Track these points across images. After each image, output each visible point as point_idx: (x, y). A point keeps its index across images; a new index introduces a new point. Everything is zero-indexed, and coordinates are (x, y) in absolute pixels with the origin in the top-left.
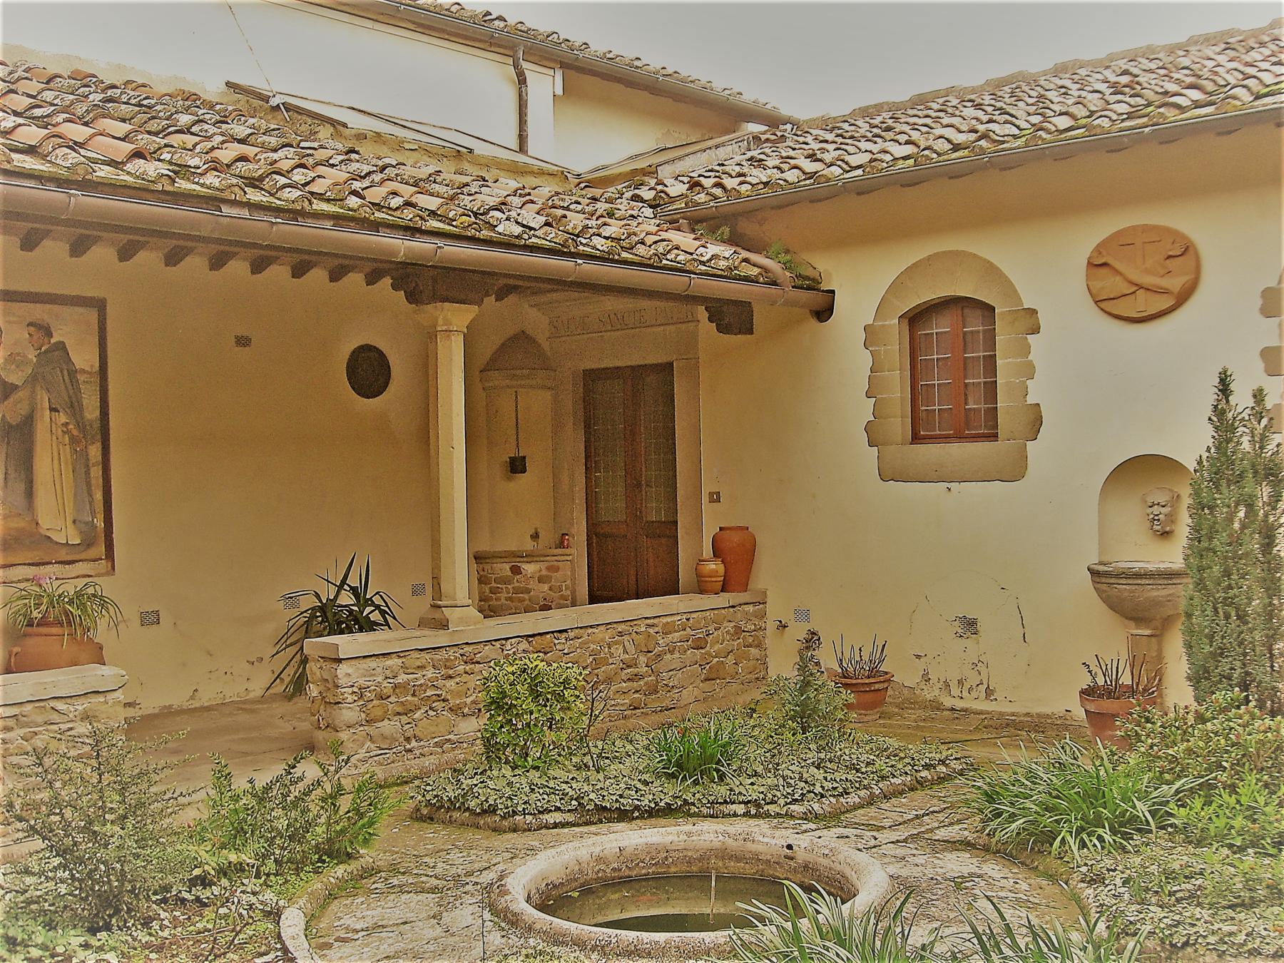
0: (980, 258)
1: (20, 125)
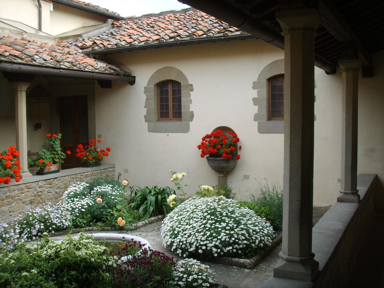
0: (177, 69)
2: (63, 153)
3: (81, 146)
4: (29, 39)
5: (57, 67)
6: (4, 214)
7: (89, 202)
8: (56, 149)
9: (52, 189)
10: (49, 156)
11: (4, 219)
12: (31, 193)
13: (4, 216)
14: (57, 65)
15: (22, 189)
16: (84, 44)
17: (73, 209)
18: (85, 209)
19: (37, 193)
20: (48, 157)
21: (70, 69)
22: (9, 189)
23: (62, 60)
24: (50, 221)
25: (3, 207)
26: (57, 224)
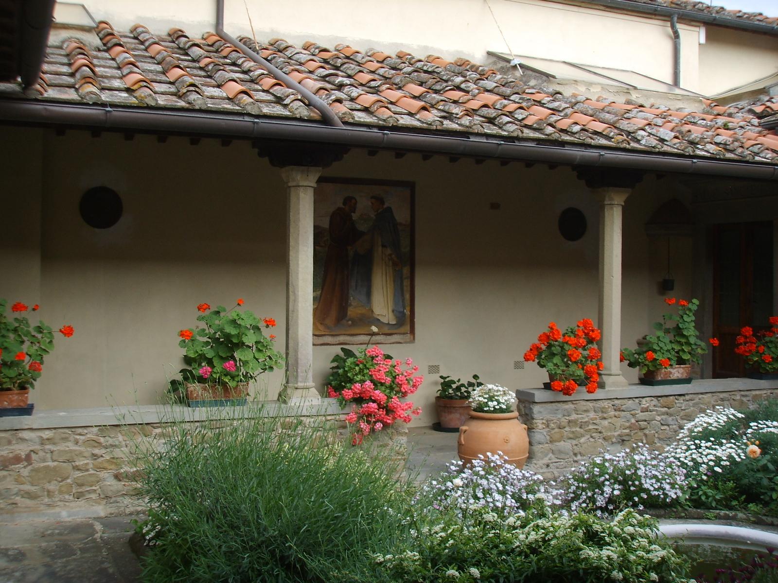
1: (361, 95)
2: (699, 342)
3: (748, 331)
4: (641, 101)
5: (687, 154)
6: (563, 456)
7: (733, 454)
8: (685, 333)
9: (671, 419)
10: (669, 347)
11: (560, 467)
12: (623, 420)
13: (562, 460)
14: (687, 150)
15: (604, 410)
16: (768, 107)
17: (697, 465)
18: (722, 467)
19: (637, 421)
20: (665, 348)
21: (718, 157)
22: (576, 406)
23: (701, 138)
24: (637, 483)
25: (560, 441)
26: (650, 491)
